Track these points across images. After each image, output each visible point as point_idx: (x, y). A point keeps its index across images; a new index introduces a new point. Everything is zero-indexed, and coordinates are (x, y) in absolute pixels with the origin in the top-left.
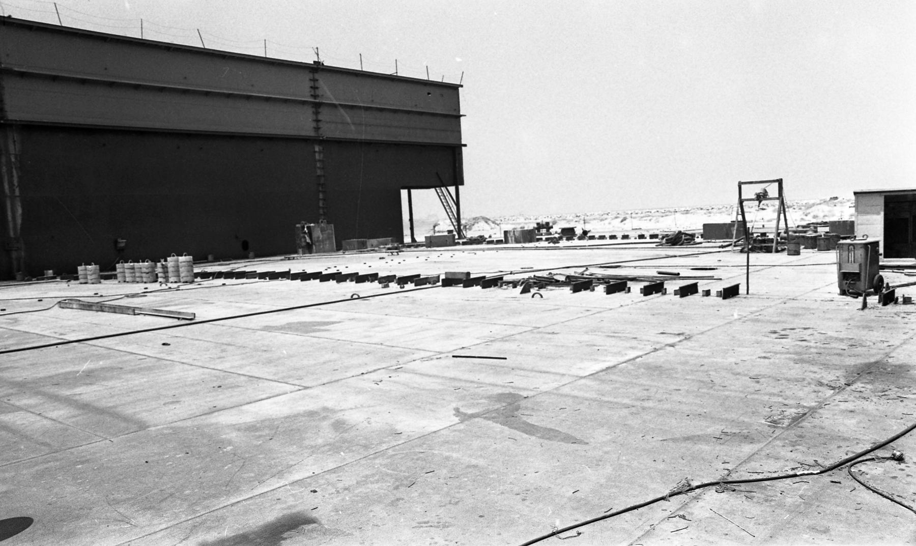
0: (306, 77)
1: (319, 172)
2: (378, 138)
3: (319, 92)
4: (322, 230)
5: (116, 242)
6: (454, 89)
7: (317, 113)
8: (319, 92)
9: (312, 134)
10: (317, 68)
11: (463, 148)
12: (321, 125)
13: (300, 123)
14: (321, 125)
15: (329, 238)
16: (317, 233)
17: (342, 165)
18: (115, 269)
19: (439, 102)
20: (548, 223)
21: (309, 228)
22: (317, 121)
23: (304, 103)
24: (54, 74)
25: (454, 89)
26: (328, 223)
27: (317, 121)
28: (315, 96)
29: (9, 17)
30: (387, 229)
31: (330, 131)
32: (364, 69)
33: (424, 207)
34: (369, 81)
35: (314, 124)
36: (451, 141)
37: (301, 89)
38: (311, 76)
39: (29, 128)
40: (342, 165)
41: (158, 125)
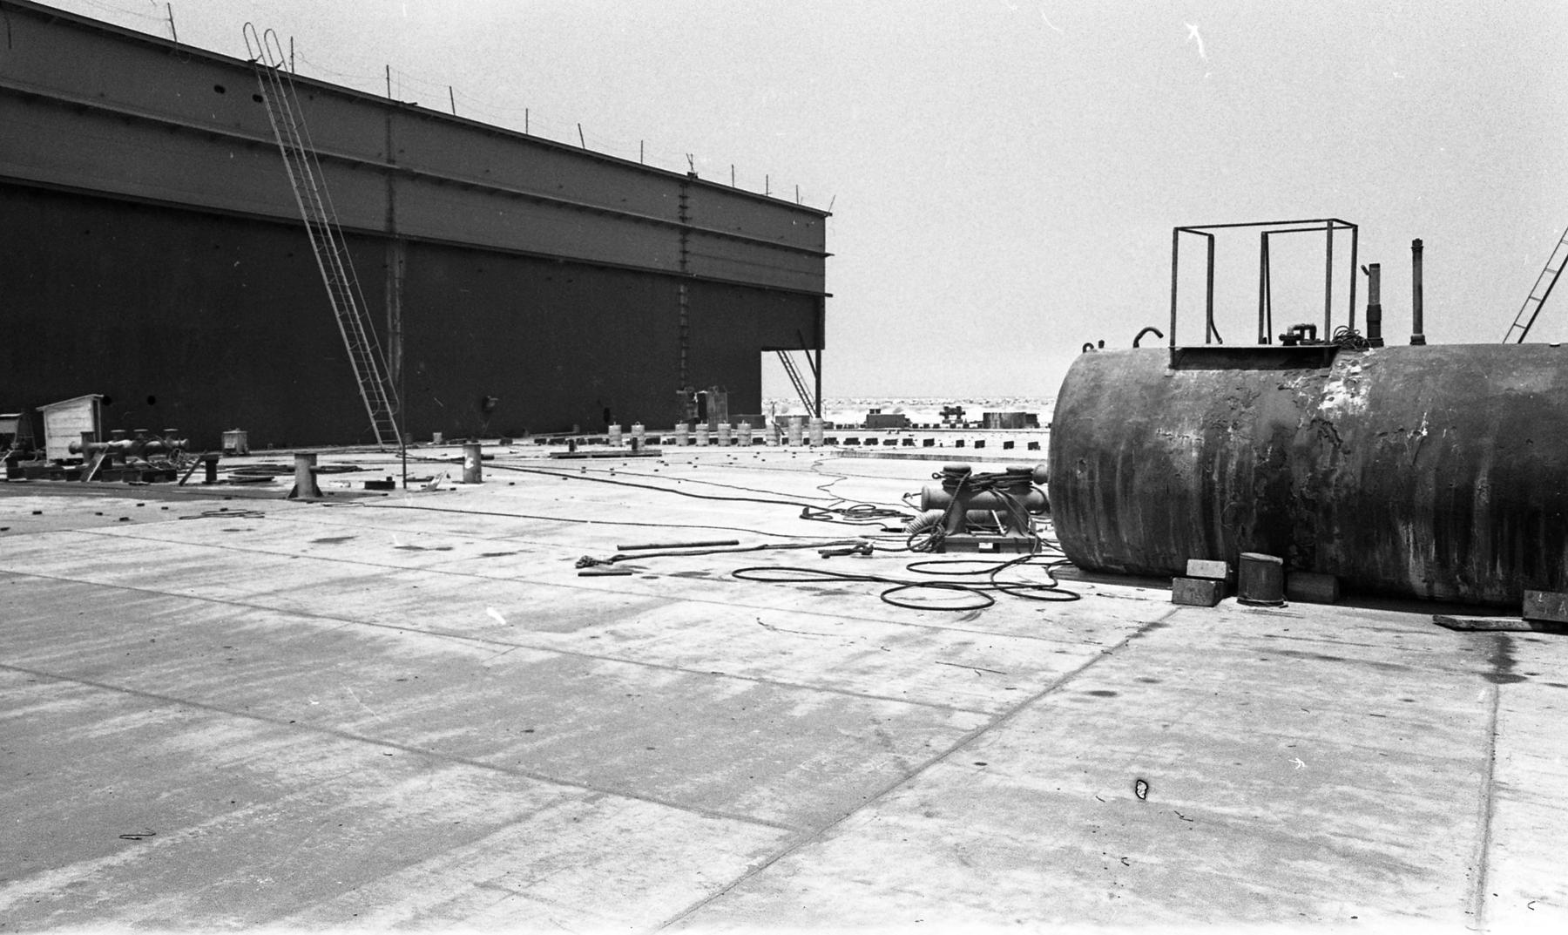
0: (676, 190)
1: (683, 321)
2: (719, 275)
3: (688, 213)
4: (717, 400)
5: (486, 401)
6: (820, 216)
7: (684, 242)
8: (688, 213)
9: (677, 268)
10: (690, 182)
11: (827, 299)
12: (688, 258)
13: (660, 253)
14: (688, 258)
15: (722, 411)
16: (711, 405)
17: (625, 305)
18: (606, 431)
19: (798, 233)
20: (959, 408)
21: (700, 396)
22: (685, 252)
23: (672, 227)
24: (29, 90)
25: (820, 216)
26: (721, 390)
27: (685, 252)
28: (683, 219)
29: (413, 105)
30: (745, 402)
31: (697, 268)
32: (394, 97)
33: (779, 378)
34: (772, 210)
35: (680, 257)
36: (812, 288)
37: (666, 206)
38: (679, 191)
39: (416, 245)
40: (625, 305)
41: (243, 206)
